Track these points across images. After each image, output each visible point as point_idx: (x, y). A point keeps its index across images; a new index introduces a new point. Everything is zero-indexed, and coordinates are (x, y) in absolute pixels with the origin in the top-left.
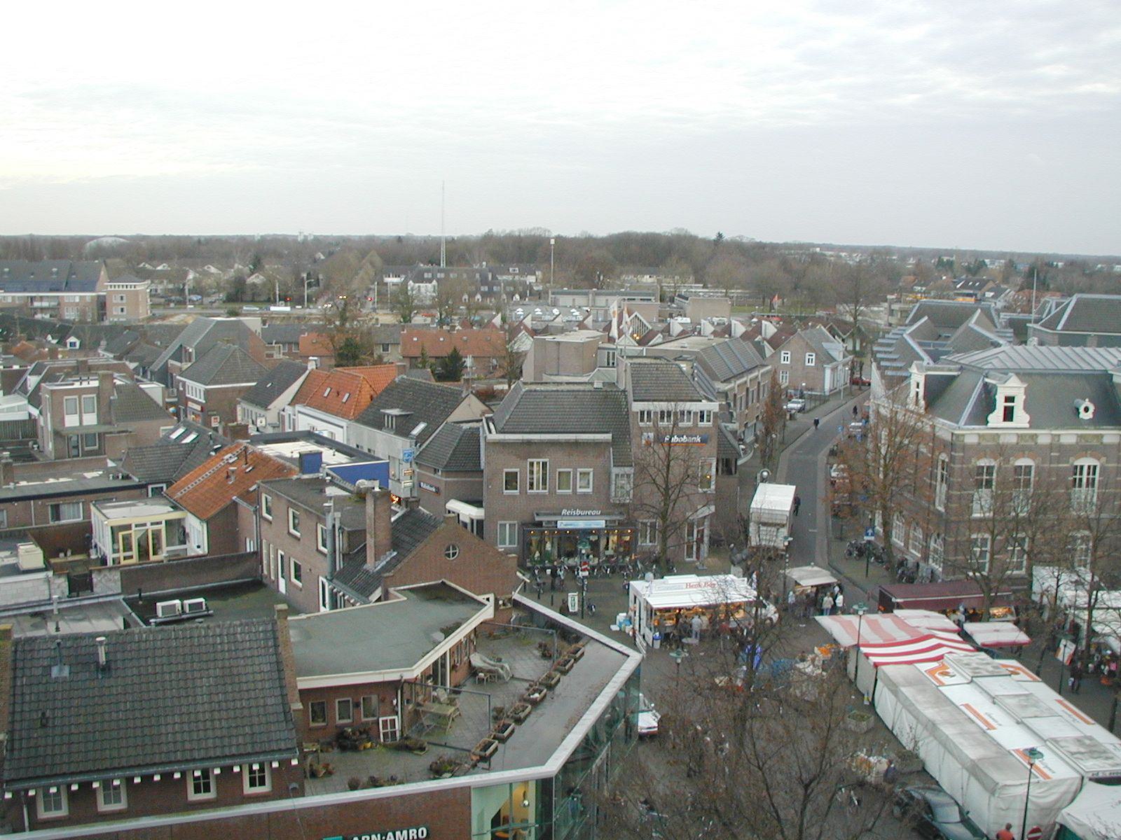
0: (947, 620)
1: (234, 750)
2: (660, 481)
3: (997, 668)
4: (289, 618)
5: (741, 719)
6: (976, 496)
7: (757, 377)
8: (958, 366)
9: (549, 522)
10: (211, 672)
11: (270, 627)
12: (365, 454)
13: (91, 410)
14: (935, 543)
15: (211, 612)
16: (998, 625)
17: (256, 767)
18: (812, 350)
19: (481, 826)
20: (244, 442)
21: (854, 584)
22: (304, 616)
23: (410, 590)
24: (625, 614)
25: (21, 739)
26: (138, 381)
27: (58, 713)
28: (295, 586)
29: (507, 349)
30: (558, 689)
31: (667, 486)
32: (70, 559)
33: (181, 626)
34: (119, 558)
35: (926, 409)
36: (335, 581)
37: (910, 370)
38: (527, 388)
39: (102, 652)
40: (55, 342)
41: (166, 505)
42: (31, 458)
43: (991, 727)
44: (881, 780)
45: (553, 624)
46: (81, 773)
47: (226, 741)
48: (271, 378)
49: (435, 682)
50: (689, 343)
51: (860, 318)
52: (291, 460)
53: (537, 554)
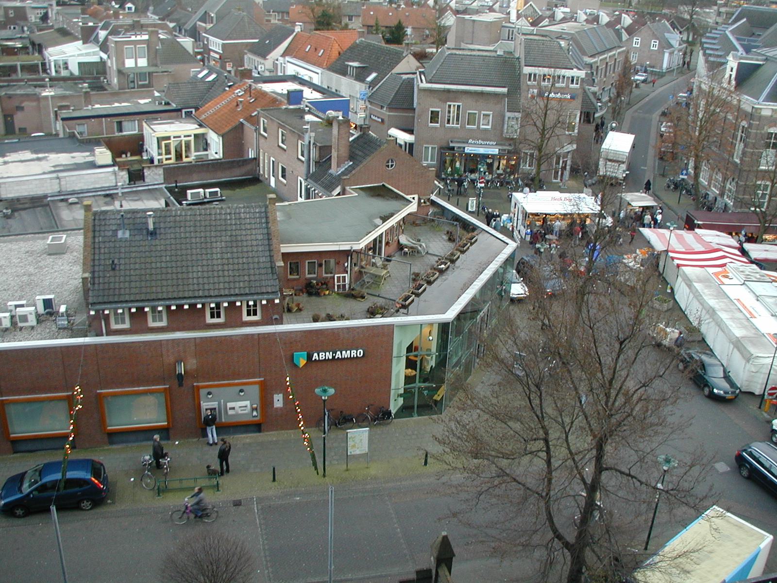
0: (732, 240)
1: (237, 291)
2: (539, 124)
3: (763, 276)
4: (277, 204)
5: (581, 293)
6: (764, 154)
7: (614, 55)
8: (764, 58)
9: (459, 148)
10: (223, 238)
11: (263, 210)
12: (333, 93)
13: (143, 55)
14: (730, 184)
15: (224, 198)
16: (768, 247)
17: (251, 303)
18: (657, 39)
19: (400, 351)
20: (249, 81)
21: (669, 208)
22: (287, 203)
23: (359, 188)
24: (507, 215)
25: (99, 277)
26: (175, 36)
27: (122, 261)
28: (281, 182)
29: (436, 24)
30: (458, 263)
31: (544, 128)
32: (130, 159)
33: (204, 207)
34: (162, 159)
35: (735, 87)
36: (309, 180)
37: (728, 58)
38: (450, 52)
39: (151, 222)
40: (117, 6)
41: (194, 123)
42: (102, 88)
43: (753, 317)
44: (673, 345)
45: (457, 218)
46: (137, 301)
47: (232, 285)
48: (269, 36)
49: (374, 252)
50: (566, 27)
51: (695, 16)
52: (281, 95)
53: (450, 169)
